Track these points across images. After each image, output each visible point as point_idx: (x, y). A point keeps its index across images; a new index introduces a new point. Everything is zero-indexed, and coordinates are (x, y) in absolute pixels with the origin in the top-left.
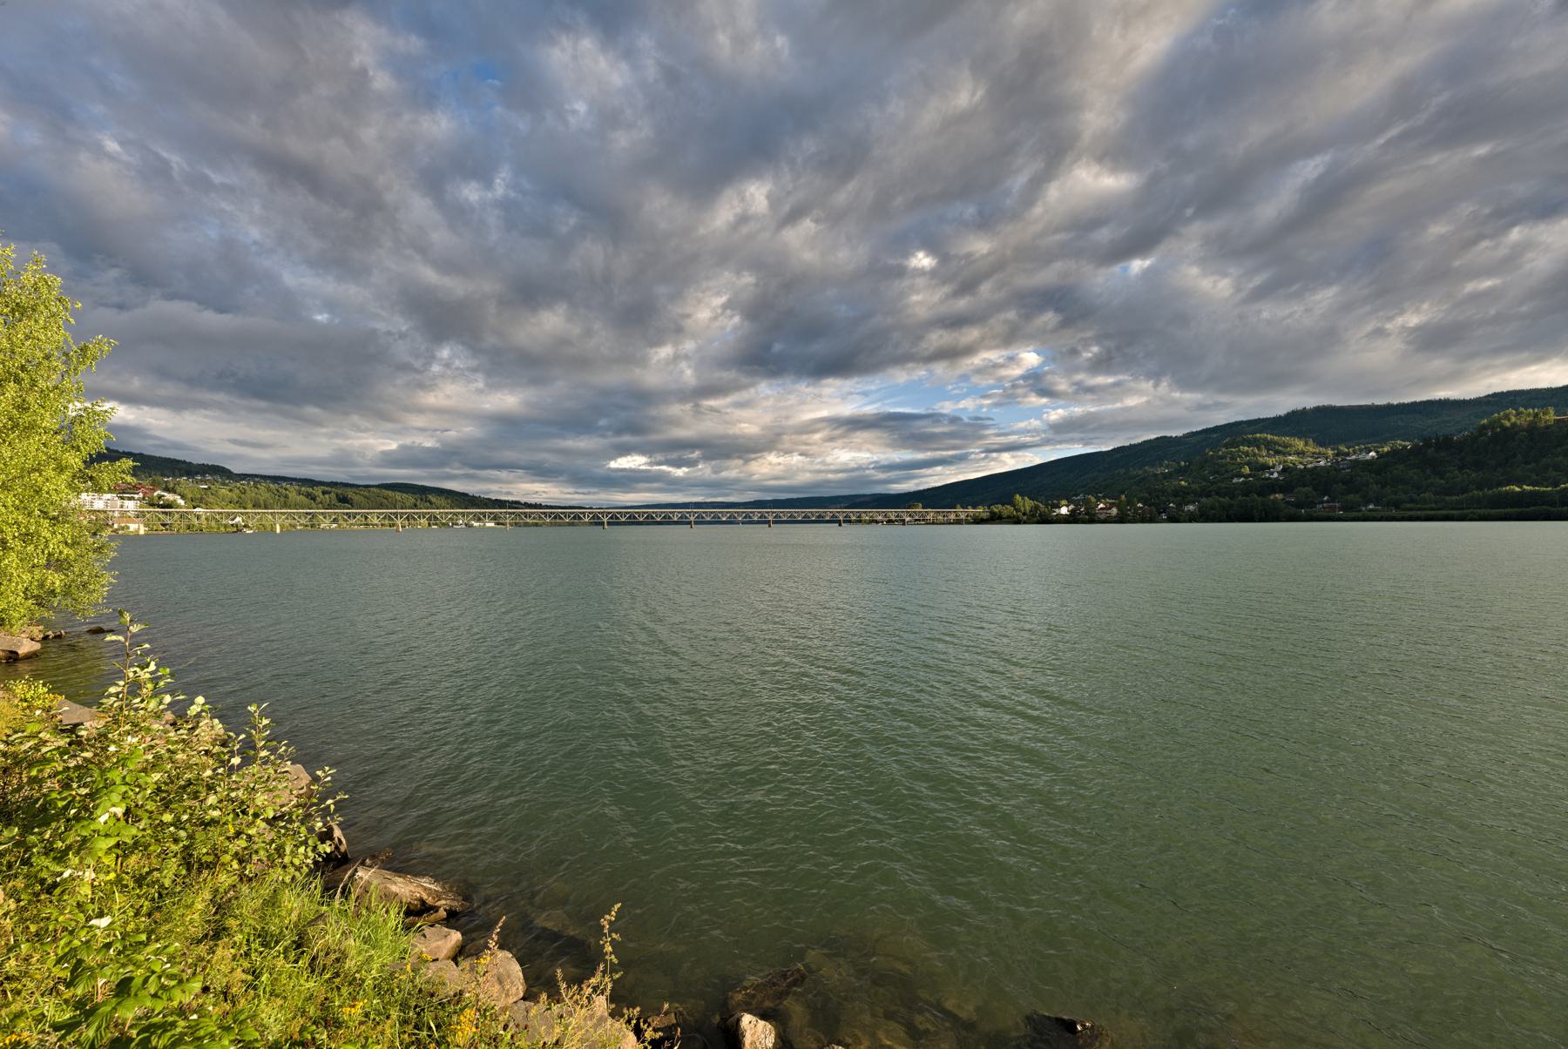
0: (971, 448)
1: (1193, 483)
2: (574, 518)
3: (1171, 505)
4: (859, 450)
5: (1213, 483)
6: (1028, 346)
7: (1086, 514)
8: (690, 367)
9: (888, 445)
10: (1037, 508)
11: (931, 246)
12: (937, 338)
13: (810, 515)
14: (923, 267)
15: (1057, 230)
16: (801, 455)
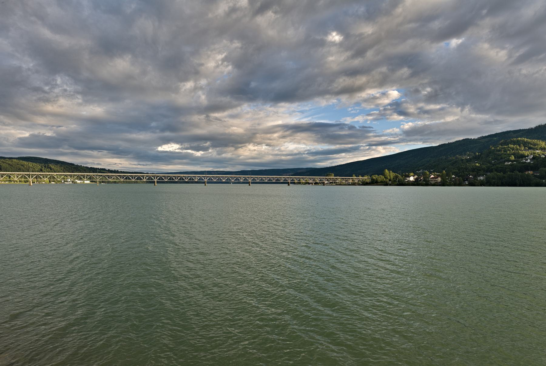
0: (361, 143)
1: (483, 164)
2: (137, 179)
3: (471, 176)
4: (299, 143)
5: (494, 165)
6: (393, 87)
7: (424, 181)
8: (204, 94)
9: (315, 141)
10: (397, 177)
11: (340, 29)
12: (343, 81)
13: (264, 179)
14: (335, 41)
15: (410, 21)
16: (267, 145)
